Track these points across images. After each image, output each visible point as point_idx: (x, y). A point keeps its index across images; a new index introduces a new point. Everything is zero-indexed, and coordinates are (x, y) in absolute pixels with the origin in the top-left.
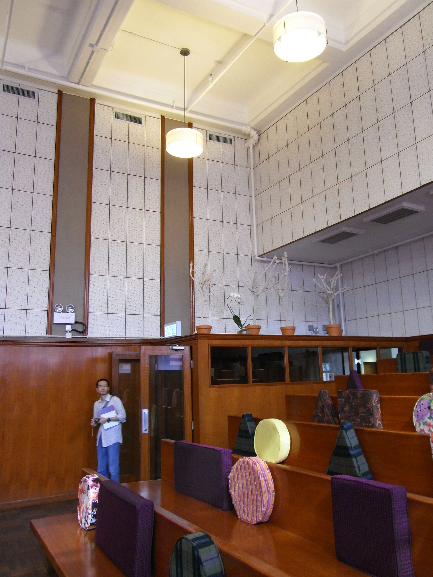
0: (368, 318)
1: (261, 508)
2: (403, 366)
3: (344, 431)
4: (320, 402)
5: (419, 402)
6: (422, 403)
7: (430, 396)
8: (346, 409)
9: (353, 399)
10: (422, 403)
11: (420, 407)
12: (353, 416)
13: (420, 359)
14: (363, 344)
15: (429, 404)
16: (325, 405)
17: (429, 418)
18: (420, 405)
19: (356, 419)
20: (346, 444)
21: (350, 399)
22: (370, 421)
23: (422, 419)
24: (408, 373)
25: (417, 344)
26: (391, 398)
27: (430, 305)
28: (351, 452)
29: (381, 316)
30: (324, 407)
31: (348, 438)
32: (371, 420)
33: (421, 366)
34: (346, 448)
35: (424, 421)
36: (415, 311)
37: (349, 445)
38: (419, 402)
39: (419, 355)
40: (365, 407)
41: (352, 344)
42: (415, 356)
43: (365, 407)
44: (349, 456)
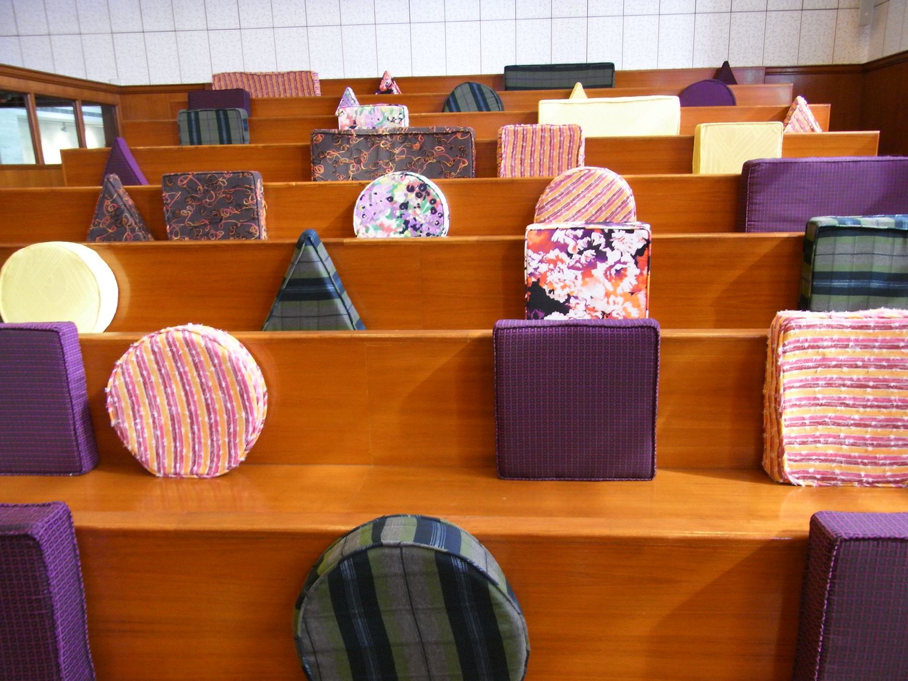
0: (83, 37)
1: (247, 436)
2: (195, 134)
3: (311, 248)
4: (108, 202)
5: (370, 189)
6: (374, 191)
7: (394, 179)
8: (187, 212)
9: (206, 192)
10: (374, 191)
11: (370, 199)
12: (205, 225)
13: (233, 123)
14: (52, 90)
15: (391, 191)
16: (123, 207)
17: (387, 217)
18: (370, 195)
19: (213, 231)
20: (318, 273)
21: (196, 191)
22: (251, 233)
23: (372, 219)
24: (203, 146)
25: (183, 97)
26: (291, 187)
27: (47, 32)
28: (330, 288)
29: (25, 38)
30: (123, 212)
31: (321, 260)
32: (252, 230)
33: (235, 134)
34: (320, 282)
35: (378, 222)
36: (269, 32)
37: (324, 275)
38: (370, 189)
39: (231, 114)
40: (239, 206)
41: (35, 87)
42: (222, 116)
43: (239, 206)
44: (328, 296)
